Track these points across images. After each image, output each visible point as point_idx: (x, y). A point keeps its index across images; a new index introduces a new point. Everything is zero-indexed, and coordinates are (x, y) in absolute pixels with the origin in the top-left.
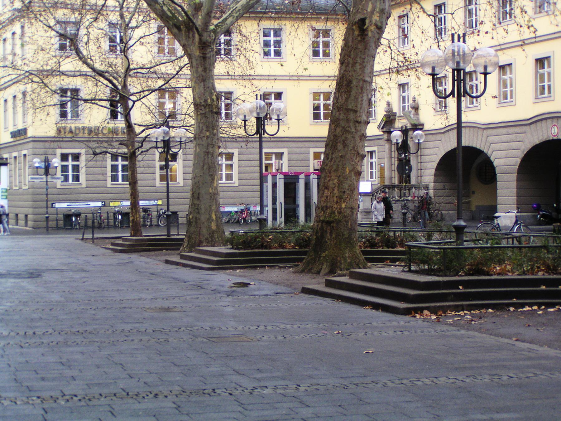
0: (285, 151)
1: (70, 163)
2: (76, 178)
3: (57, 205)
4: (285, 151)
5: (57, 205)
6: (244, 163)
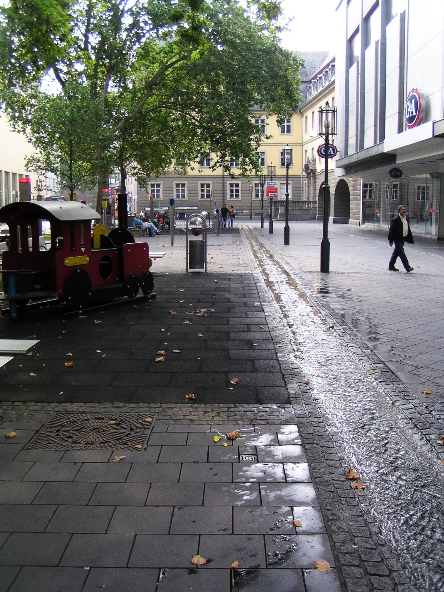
0: (161, 183)
1: (156, 188)
2: (237, 196)
3: (244, 212)
4: (186, 183)
5: (244, 212)
6: (244, 189)
